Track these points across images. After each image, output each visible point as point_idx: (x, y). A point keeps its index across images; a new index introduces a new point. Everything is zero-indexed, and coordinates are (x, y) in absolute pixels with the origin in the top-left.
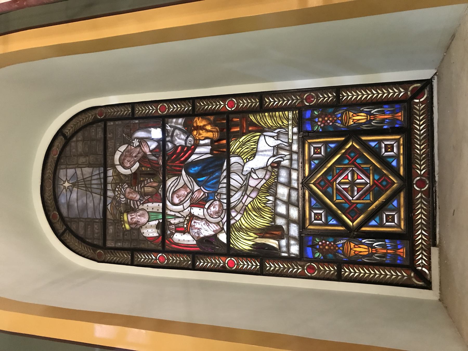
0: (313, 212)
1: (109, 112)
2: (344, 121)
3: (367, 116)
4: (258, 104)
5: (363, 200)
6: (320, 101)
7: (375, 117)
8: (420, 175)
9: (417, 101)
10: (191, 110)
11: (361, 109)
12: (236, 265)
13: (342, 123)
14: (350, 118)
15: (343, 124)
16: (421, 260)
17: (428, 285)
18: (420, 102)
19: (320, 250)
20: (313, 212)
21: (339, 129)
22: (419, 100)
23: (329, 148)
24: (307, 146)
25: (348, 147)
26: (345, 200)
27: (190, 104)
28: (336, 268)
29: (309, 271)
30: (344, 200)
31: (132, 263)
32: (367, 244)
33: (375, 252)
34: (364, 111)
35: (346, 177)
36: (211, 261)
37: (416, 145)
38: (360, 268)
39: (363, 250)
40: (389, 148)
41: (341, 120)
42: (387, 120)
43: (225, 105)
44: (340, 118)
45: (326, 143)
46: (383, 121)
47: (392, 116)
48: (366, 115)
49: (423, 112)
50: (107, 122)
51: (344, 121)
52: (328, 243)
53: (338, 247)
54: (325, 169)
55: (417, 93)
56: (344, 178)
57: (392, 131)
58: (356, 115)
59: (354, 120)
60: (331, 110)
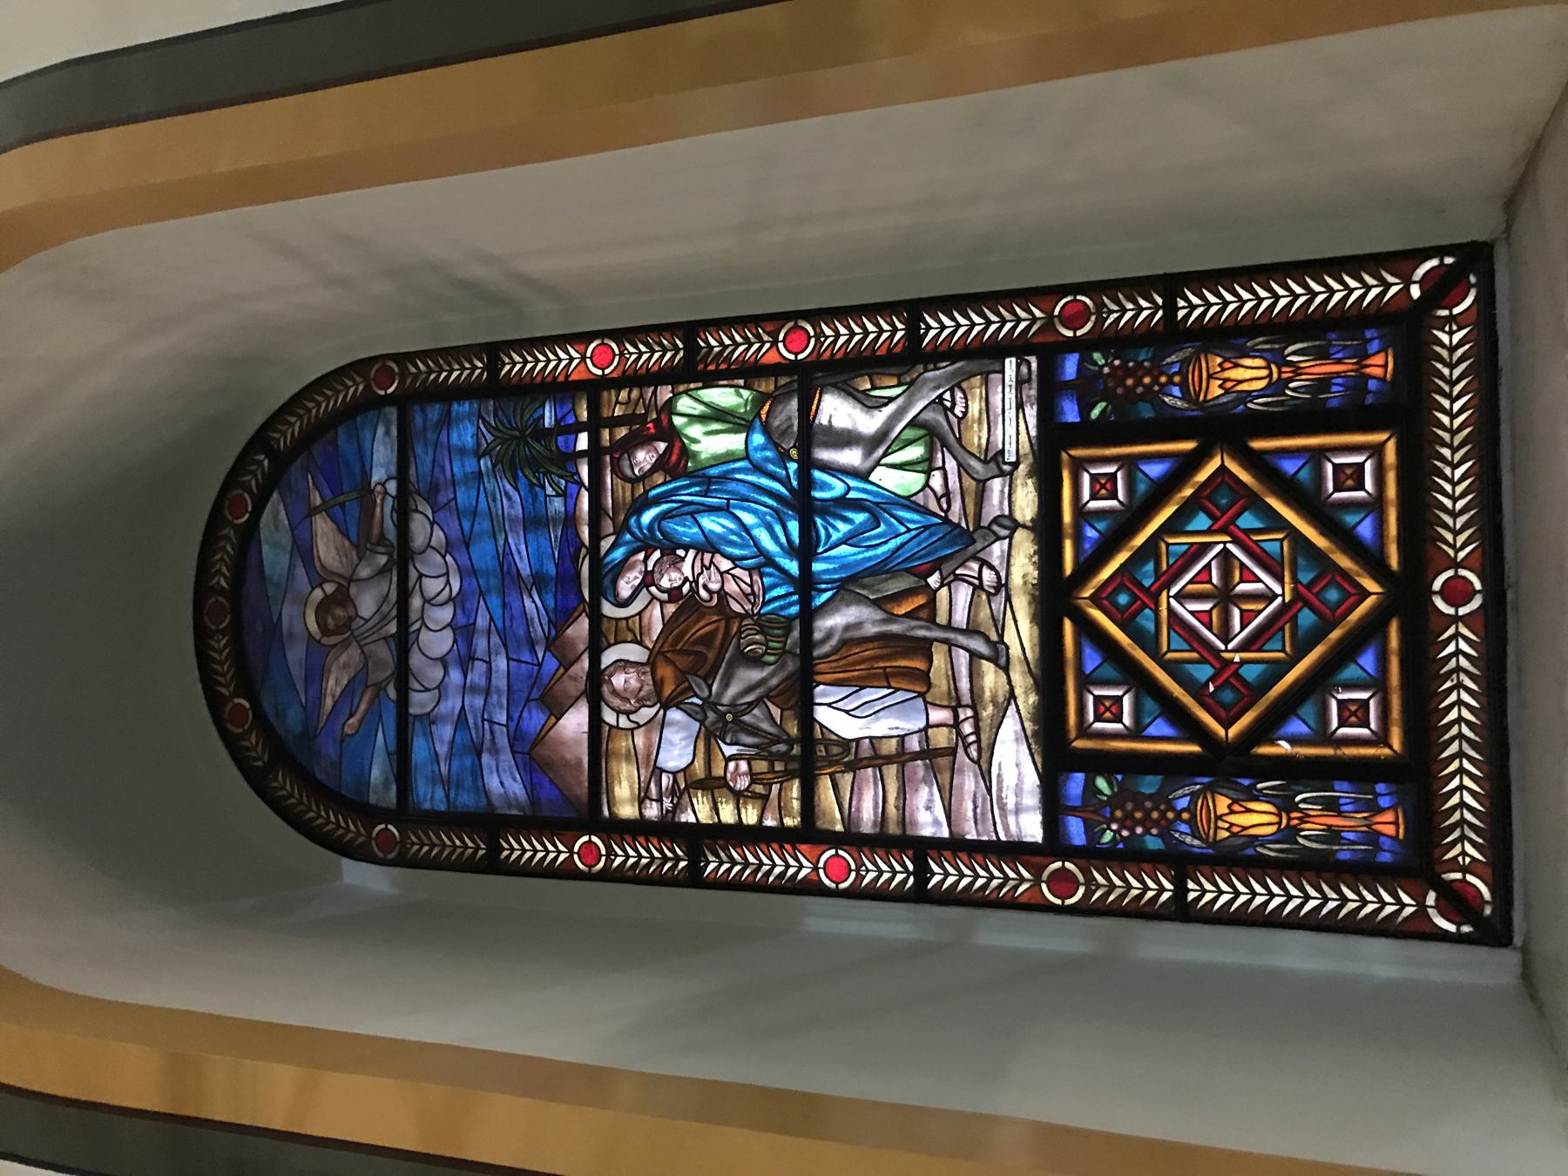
0: (1088, 502)
2: (1191, 388)
3: (1280, 816)
6: (1109, 321)
9: (1444, 313)
14: (1210, 376)
15: (1200, 838)
16: (1458, 777)
20: (1088, 502)
21: (1179, 414)
25: (1202, 476)
26: (1199, 650)
34: (1258, 351)
35: (1204, 577)
36: (744, 857)
38: (1251, 879)
39: (1259, 819)
41: (1184, 386)
42: (1339, 381)
44: (1185, 816)
45: (1129, 463)
46: (1324, 383)
47: (1354, 367)
49: (1465, 353)
51: (1191, 388)
53: (1173, 809)
55: (1442, 288)
56: (1195, 580)
57: (1355, 416)
58: (1242, 809)
59: (1226, 380)
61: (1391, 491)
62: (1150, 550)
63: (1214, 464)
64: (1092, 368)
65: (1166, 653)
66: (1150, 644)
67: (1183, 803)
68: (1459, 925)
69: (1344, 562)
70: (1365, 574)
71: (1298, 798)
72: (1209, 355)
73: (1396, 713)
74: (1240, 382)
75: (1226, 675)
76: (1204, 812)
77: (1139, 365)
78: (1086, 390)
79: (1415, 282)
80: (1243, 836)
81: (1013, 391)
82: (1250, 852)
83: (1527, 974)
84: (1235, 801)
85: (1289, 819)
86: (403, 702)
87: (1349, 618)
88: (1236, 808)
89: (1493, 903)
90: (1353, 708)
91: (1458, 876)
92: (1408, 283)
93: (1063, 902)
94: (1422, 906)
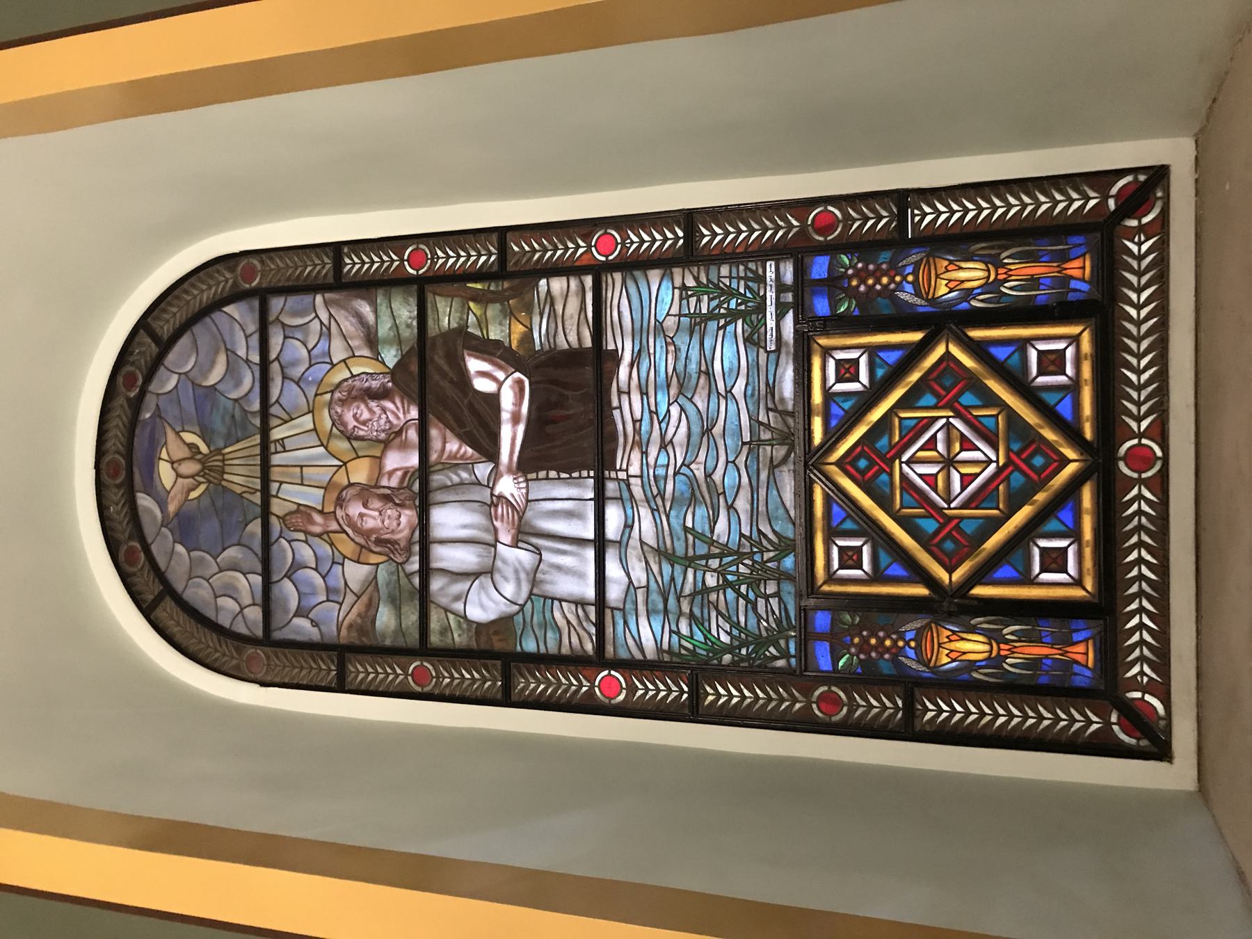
1: (271, 270)
3: (989, 271)
5: (977, 508)
7: (1010, 273)
8: (1141, 482)
9: (1134, 223)
10: (496, 263)
12: (619, 246)
13: (918, 294)
17: (1161, 750)
22: (1140, 222)
23: (881, 367)
24: (816, 363)
27: (491, 248)
28: (895, 210)
29: (823, 705)
30: (923, 508)
31: (341, 687)
32: (983, 632)
33: (1005, 276)
34: (977, 255)
37: (1126, 403)
40: (1052, 362)
43: (589, 251)
45: (872, 350)
46: (1033, 282)
48: (987, 641)
50: (267, 296)
52: (871, 267)
60: (885, 256)
62: (883, 425)
63: (939, 351)
64: (844, 626)
66: (884, 502)
67: (909, 269)
68: (1138, 739)
69: (1049, 435)
70: (1065, 445)
72: (937, 260)
73: (1088, 563)
75: (948, 528)
76: (925, 273)
77: (878, 268)
78: (833, 284)
79: (1112, 196)
81: (774, 290)
82: (965, 676)
84: (951, 262)
85: (999, 649)
86: (265, 431)
87: (1052, 483)
88: (953, 638)
90: (1054, 555)
91: (1138, 695)
94: (1108, 724)
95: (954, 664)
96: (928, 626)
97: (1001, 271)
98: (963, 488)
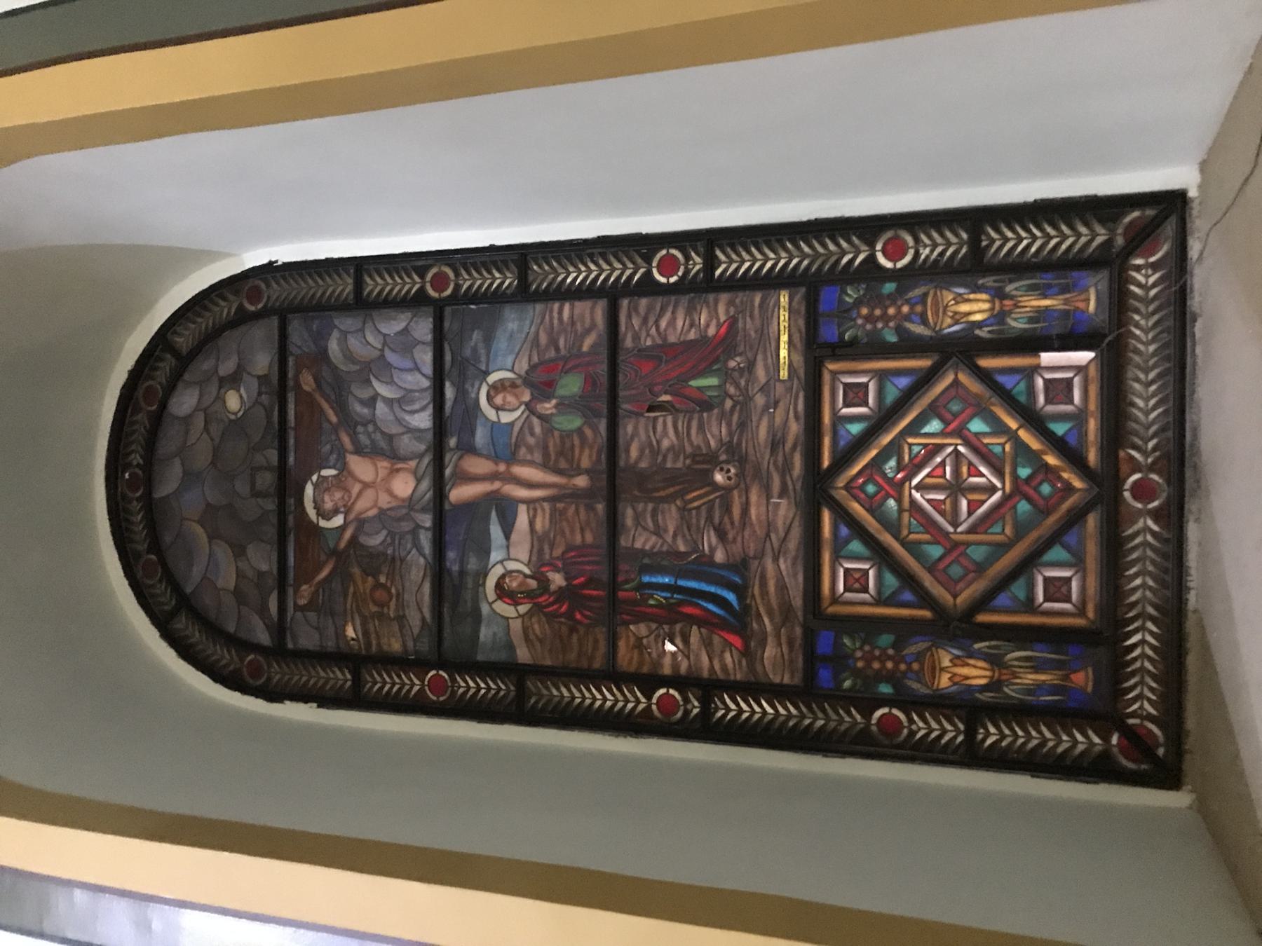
4: (964, 250)
11: (980, 282)
18: (1148, 266)
19: (856, 673)
30: (928, 533)
35: (939, 472)
45: (882, 376)
54: (874, 453)
55: (1140, 239)
61: (1093, 406)
62: (894, 448)
65: (1006, 443)
66: (893, 527)
71: (1010, 656)
74: (969, 314)
80: (963, 685)
83: (1202, 807)
85: (1000, 674)
88: (959, 299)
89: (1166, 745)
92: (1112, 231)
93: (668, 691)
95: (955, 687)
96: (929, 649)
97: (1007, 302)
98: (970, 513)
